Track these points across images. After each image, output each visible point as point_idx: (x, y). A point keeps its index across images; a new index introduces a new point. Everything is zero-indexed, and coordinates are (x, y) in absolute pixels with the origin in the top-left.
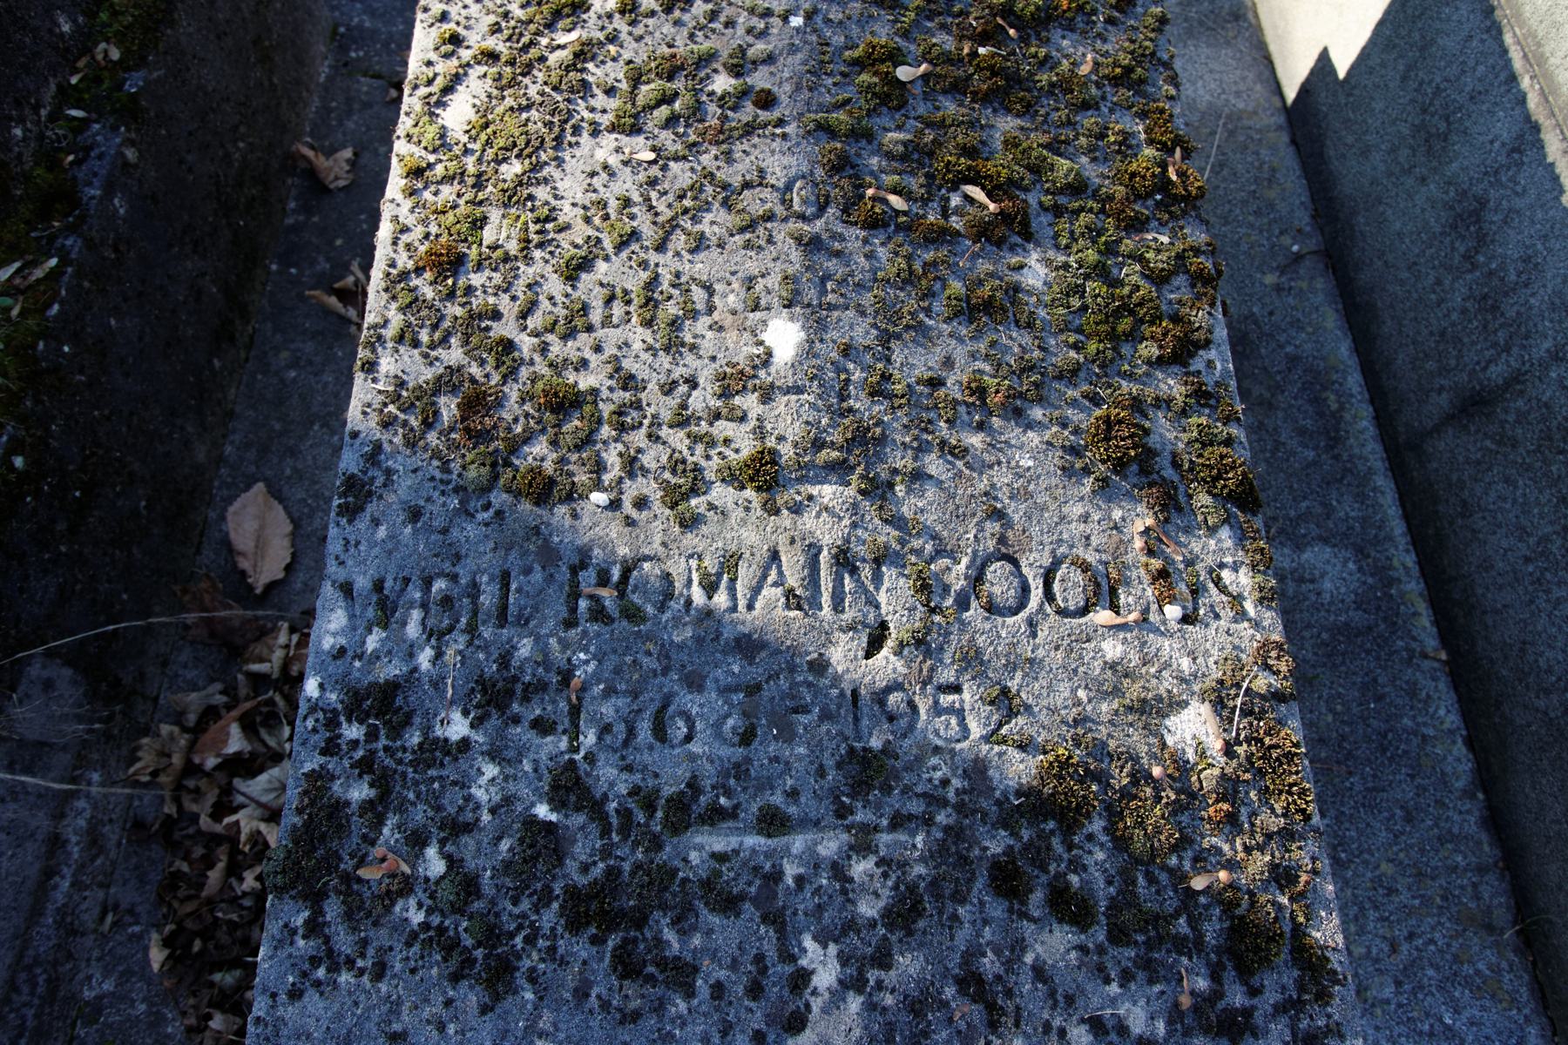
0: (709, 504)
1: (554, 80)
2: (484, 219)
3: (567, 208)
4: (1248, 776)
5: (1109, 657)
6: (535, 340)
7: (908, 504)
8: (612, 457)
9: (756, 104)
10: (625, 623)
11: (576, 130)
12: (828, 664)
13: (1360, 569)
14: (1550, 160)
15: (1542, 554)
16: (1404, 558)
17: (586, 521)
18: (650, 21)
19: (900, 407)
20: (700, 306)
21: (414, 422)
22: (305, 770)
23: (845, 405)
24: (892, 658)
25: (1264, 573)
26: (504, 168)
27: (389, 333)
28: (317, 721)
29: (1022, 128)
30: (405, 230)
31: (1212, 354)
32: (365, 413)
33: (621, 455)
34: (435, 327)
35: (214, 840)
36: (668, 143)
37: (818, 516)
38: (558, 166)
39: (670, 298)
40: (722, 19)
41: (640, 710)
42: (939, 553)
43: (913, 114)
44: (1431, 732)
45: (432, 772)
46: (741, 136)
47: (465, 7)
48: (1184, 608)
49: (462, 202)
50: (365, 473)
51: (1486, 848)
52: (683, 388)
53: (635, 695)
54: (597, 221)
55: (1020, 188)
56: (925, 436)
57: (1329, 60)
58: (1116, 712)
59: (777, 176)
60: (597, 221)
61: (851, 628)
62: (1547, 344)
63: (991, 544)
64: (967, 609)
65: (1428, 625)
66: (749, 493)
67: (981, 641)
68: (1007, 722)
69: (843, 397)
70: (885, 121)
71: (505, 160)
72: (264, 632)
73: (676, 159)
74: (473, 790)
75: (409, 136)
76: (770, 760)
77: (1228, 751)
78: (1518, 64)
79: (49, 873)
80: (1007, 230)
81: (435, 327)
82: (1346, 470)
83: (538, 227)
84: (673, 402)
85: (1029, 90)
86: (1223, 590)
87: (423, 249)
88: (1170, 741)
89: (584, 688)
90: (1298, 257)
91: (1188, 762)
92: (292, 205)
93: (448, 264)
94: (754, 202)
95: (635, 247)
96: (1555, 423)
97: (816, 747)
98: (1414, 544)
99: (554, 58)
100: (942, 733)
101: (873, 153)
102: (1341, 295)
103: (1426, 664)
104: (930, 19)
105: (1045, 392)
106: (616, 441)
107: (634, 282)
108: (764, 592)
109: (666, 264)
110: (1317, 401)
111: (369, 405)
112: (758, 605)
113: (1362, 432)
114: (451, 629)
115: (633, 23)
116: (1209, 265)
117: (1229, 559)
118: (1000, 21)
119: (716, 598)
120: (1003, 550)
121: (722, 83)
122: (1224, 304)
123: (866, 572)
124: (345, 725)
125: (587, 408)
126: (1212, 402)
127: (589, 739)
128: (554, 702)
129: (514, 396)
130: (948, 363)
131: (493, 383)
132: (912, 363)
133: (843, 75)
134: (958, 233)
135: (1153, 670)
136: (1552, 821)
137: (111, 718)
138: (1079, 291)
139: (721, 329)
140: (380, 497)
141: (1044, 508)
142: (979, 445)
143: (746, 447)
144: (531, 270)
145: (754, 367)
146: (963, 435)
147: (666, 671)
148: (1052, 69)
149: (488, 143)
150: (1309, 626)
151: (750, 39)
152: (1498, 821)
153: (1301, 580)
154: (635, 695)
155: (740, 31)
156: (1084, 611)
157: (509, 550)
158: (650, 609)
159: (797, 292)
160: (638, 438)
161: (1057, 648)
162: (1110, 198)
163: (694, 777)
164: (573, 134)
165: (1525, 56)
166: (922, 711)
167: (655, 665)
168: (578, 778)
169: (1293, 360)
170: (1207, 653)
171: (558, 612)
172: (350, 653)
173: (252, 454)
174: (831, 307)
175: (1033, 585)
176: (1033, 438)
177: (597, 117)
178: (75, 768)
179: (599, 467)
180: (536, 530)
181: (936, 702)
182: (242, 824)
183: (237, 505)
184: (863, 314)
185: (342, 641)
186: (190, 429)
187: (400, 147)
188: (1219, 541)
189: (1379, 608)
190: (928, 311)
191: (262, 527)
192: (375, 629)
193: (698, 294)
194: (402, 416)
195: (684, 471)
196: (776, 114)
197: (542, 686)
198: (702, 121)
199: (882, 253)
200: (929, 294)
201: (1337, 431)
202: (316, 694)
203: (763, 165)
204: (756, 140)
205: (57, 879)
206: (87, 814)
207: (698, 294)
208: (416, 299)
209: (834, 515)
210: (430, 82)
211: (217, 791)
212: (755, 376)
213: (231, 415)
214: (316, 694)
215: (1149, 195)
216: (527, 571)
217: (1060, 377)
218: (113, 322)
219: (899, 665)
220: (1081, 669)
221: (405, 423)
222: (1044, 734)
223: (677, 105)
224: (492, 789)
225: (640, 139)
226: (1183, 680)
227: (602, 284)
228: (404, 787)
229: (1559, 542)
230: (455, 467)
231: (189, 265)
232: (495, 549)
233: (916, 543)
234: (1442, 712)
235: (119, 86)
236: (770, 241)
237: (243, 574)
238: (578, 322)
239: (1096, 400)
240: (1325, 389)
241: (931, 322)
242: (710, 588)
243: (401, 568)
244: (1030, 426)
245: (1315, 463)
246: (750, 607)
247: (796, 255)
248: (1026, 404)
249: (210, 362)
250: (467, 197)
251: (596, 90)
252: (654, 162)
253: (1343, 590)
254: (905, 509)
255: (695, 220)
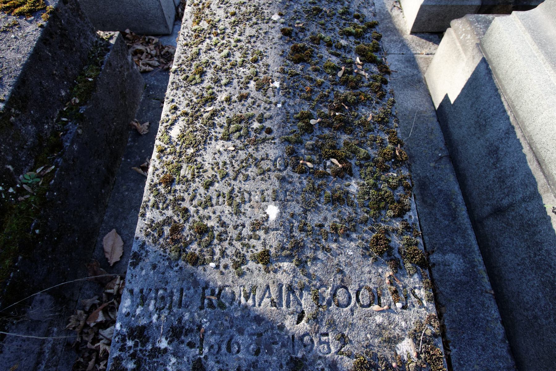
0: (248, 268)
1: (205, 122)
2: (181, 167)
3: (207, 164)
4: (425, 366)
5: (378, 322)
6: (195, 209)
7: (312, 269)
8: (217, 250)
9: (266, 132)
10: (219, 309)
11: (211, 139)
12: (284, 326)
13: (464, 262)
14: (518, 138)
15: (523, 263)
16: (478, 258)
17: (208, 272)
18: (235, 104)
19: (310, 235)
20: (247, 200)
21: (156, 235)
22: (114, 356)
23: (292, 234)
24: (306, 324)
25: (429, 291)
26: (188, 150)
27: (150, 204)
28: (119, 338)
29: (350, 139)
30: (157, 169)
31: (411, 213)
32: (141, 231)
33: (220, 250)
34: (164, 203)
35: (91, 351)
36: (239, 144)
37: (282, 274)
38: (205, 150)
39: (237, 196)
40: (257, 104)
41: (223, 341)
42: (322, 286)
43: (315, 135)
44: (490, 319)
45: (155, 360)
46: (261, 143)
47: (179, 98)
48: (403, 304)
49: (174, 161)
50: (140, 251)
51: (510, 361)
52: (240, 228)
53: (222, 335)
54: (216, 169)
55: (349, 159)
56: (318, 245)
57: (448, 98)
58: (380, 342)
59: (272, 157)
60: (216, 169)
61: (292, 313)
62: (521, 196)
63: (339, 282)
64: (331, 306)
65: (487, 281)
66: (260, 265)
67: (335, 317)
68: (344, 347)
69: (291, 232)
70: (306, 137)
71: (188, 148)
72: (113, 279)
73: (241, 150)
74: (167, 367)
75: (160, 139)
76: (265, 361)
77: (418, 357)
78: (506, 107)
79: (38, 363)
80: (345, 173)
81: (164, 203)
82: (458, 228)
83: (197, 171)
84: (237, 232)
85: (352, 126)
86: (416, 296)
87: (162, 176)
88: (398, 353)
89: (205, 332)
90: (441, 158)
91: (404, 360)
92: (130, 139)
93: (169, 182)
94: (265, 165)
95: (227, 178)
96: (524, 222)
97: (280, 357)
98: (481, 253)
99: (205, 115)
100: (322, 351)
101: (302, 148)
102: (455, 170)
103: (487, 295)
104: (321, 103)
105: (356, 228)
106: (219, 244)
107: (226, 190)
108: (264, 300)
109: (237, 185)
110: (448, 205)
111: (142, 228)
112: (262, 304)
113: (463, 215)
114: (163, 308)
115: (229, 105)
116: (410, 183)
117: (417, 286)
118: (343, 104)
119: (248, 301)
120: (343, 284)
121: (256, 125)
122: (414, 195)
123: (298, 293)
124: (128, 341)
125: (210, 233)
126: (411, 230)
127: (206, 350)
128: (195, 336)
129: (187, 228)
130: (325, 219)
131: (181, 223)
132: (314, 219)
133: (294, 123)
134: (329, 174)
135: (392, 327)
136: (531, 355)
137: (62, 310)
138: (368, 193)
139: (253, 207)
140: (144, 260)
141: (356, 269)
142: (335, 247)
143: (260, 249)
144: (195, 185)
145: (263, 221)
146: (330, 244)
147: (232, 327)
148: (359, 119)
149: (184, 142)
150: (448, 281)
151: (265, 111)
152: (513, 351)
153: (445, 265)
154: (222, 335)
155: (262, 108)
156: (369, 305)
157: (183, 281)
158: (227, 304)
159: (277, 196)
160: (226, 244)
161: (360, 319)
162: (378, 161)
163: (239, 366)
164: (210, 140)
165: (508, 105)
166: (315, 343)
167: (228, 325)
168: (202, 365)
169: (440, 191)
170: (410, 320)
171: (198, 304)
172: (131, 315)
173: (112, 219)
174: (288, 201)
175: (352, 296)
176: (353, 244)
177: (217, 135)
178: (49, 327)
179: (213, 253)
180: (192, 274)
181: (320, 339)
182: (101, 347)
183: (107, 236)
184: (298, 203)
185: (129, 310)
186: (93, 213)
187: (157, 142)
188: (414, 279)
189: (471, 275)
190: (319, 201)
191: (114, 244)
192: (140, 306)
193: (246, 195)
194: (152, 233)
195: (240, 256)
196: (272, 136)
197: (191, 330)
198: (249, 137)
199: (305, 182)
200: (320, 195)
201: (455, 215)
202: (119, 329)
203: (268, 153)
204: (266, 144)
205: (40, 365)
206: (52, 342)
207: (246, 195)
208: (159, 193)
209: (287, 273)
210: (167, 122)
211: (94, 334)
212: (263, 224)
213: (107, 206)
214: (119, 329)
215: (390, 160)
216: (189, 289)
217: (361, 223)
218: (71, 183)
219: (308, 326)
220: (368, 327)
221: (153, 235)
222: (356, 351)
223: (242, 132)
224: (174, 367)
225: (230, 143)
226: (403, 330)
227: (216, 191)
228: (145, 364)
229: (528, 261)
230: (168, 251)
231: (96, 162)
232: (179, 280)
233: (314, 283)
234: (493, 312)
235: (78, 111)
236: (269, 178)
237: (107, 259)
238: (208, 204)
239: (373, 231)
240: (451, 201)
241: (320, 205)
242: (247, 298)
243: (149, 285)
244: (351, 240)
245: (448, 225)
246: (260, 305)
247: (277, 183)
248: (351, 233)
249: (101, 191)
250: (176, 160)
251: (217, 126)
252: (234, 150)
253: (459, 269)
254: (310, 271)
255: (246, 170)
